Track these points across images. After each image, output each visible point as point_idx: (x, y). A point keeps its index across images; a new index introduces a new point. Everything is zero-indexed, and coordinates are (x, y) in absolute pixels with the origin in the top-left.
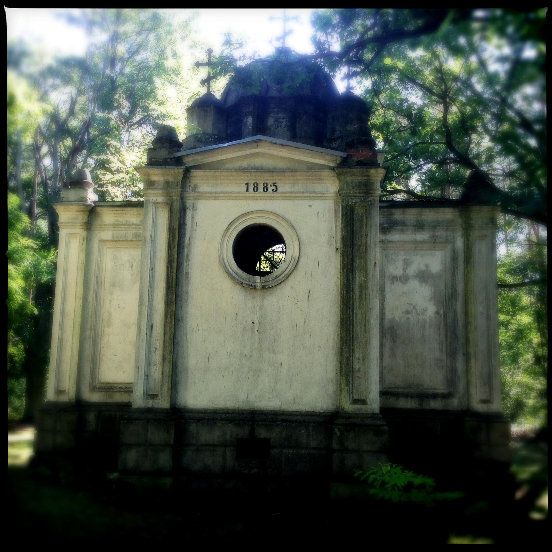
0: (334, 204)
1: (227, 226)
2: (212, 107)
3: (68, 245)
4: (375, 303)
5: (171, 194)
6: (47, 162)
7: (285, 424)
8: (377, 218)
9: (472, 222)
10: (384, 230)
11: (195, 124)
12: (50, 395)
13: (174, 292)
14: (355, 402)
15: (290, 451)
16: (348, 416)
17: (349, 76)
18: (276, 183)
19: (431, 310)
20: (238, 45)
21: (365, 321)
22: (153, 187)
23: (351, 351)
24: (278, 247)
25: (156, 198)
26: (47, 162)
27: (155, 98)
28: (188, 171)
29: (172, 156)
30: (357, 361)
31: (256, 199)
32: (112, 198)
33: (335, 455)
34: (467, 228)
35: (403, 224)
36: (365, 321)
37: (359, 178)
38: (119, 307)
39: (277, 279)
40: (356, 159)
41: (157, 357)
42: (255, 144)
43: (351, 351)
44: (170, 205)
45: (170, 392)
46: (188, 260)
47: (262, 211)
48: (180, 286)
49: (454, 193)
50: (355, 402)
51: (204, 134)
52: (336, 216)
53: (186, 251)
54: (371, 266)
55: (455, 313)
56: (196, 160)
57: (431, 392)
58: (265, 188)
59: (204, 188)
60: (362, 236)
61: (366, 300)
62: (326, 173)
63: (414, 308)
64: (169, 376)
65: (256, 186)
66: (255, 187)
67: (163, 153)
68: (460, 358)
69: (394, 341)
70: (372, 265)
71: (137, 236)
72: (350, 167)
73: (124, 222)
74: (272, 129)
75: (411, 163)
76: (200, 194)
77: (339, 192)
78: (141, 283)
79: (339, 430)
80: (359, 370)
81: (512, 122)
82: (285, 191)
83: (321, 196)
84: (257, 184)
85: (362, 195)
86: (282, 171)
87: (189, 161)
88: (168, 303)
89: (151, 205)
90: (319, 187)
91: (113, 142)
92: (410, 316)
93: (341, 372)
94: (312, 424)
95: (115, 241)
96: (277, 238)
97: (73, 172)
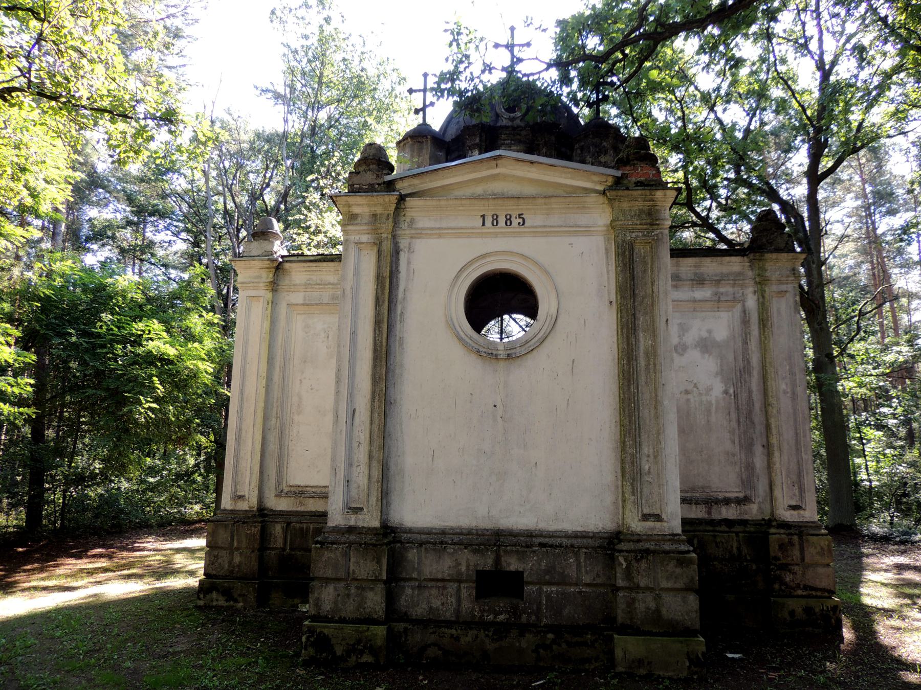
0: (605, 241)
1: (455, 274)
2: (429, 137)
5: (379, 231)
7: (544, 549)
9: (768, 274)
13: (384, 363)
14: (646, 517)
15: (553, 589)
16: (638, 538)
18: (522, 214)
19: (718, 388)
21: (656, 403)
22: (355, 222)
23: (638, 445)
25: (359, 236)
28: (402, 198)
29: (381, 181)
30: (646, 459)
31: (496, 235)
33: (621, 595)
34: (761, 282)
36: (656, 403)
38: (312, 389)
39: (527, 346)
40: (633, 179)
41: (361, 455)
42: (494, 163)
43: (638, 444)
44: (378, 244)
45: (379, 503)
46: (402, 321)
48: (392, 357)
50: (646, 517)
52: (607, 257)
53: (399, 308)
55: (750, 392)
56: (414, 185)
57: (721, 496)
58: (508, 222)
60: (646, 284)
61: (655, 373)
62: (593, 199)
63: (695, 386)
64: (378, 482)
65: (495, 218)
66: (494, 219)
67: (369, 177)
68: (758, 450)
70: (663, 324)
72: (627, 189)
73: (318, 282)
76: (419, 231)
77: (612, 225)
79: (626, 560)
80: (649, 472)
82: (535, 224)
83: (587, 231)
84: (497, 216)
85: (645, 227)
87: (404, 187)
88: (375, 381)
89: (353, 245)
90: (583, 219)
92: (689, 396)
93: (623, 476)
94: (584, 550)
95: (308, 304)
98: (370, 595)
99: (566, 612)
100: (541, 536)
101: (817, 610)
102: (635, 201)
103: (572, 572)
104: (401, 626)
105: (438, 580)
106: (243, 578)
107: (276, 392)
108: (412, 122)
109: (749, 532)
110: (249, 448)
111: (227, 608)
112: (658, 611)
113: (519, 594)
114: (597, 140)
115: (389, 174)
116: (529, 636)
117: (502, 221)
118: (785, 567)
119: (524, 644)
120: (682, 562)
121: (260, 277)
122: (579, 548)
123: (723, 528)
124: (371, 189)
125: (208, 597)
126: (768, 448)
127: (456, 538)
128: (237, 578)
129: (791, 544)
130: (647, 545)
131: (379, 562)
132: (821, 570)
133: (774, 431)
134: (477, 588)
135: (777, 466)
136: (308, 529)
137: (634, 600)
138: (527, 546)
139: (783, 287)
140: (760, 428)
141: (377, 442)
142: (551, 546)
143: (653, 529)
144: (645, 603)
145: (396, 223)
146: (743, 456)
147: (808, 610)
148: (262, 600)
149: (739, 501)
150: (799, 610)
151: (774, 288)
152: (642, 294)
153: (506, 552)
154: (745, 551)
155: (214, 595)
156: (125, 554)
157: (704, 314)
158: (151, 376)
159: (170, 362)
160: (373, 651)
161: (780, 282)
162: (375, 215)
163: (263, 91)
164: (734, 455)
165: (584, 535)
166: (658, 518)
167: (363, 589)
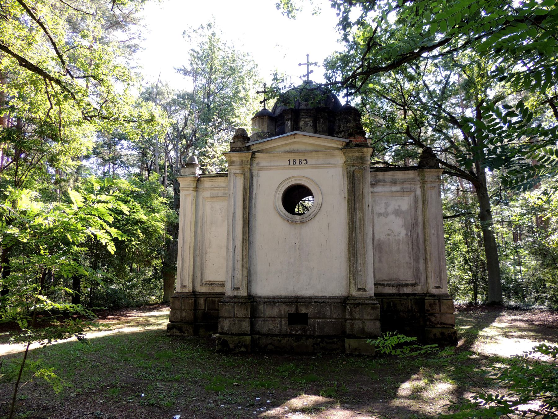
3: (185, 200)
4: (369, 230)
6: (172, 154)
8: (369, 178)
10: (373, 185)
11: (257, 127)
12: (178, 288)
14: (359, 290)
16: (355, 298)
17: (347, 95)
19: (403, 232)
20: (281, 81)
23: (356, 259)
24: (310, 197)
26: (172, 154)
27: (233, 114)
28: (254, 153)
29: (244, 146)
31: (295, 169)
32: (209, 172)
34: (423, 182)
35: (384, 181)
37: (357, 154)
40: (354, 143)
41: (239, 266)
42: (293, 137)
44: (244, 174)
46: (255, 207)
47: (299, 176)
49: (413, 163)
50: (359, 290)
51: (263, 132)
53: (254, 201)
54: (366, 207)
55: (418, 234)
57: (404, 283)
58: (300, 162)
59: (263, 163)
62: (337, 152)
63: (392, 232)
65: (295, 161)
67: (239, 144)
68: (422, 261)
69: (380, 252)
70: (367, 207)
71: (224, 194)
72: (351, 148)
74: (303, 127)
75: (385, 146)
78: (228, 222)
80: (361, 271)
81: (445, 118)
83: (334, 166)
86: (311, 152)
88: (244, 233)
89: (233, 175)
90: (333, 161)
91: (210, 141)
92: (390, 237)
96: (308, 192)
97: (187, 159)
98: (244, 323)
99: (326, 330)
100: (315, 298)
101: (446, 334)
102: (355, 153)
103: (328, 313)
104: (257, 337)
105: (272, 317)
106: (187, 322)
107: (199, 239)
108: (258, 108)
109: (416, 299)
110: (188, 264)
111: (181, 336)
112: (363, 328)
113: (306, 323)
114: (346, 116)
115: (248, 143)
116: (310, 340)
117: (297, 162)
118: (432, 314)
119: (308, 343)
120: (373, 308)
121: (190, 185)
122: (331, 303)
123: (405, 297)
124: (240, 150)
125: (172, 331)
126: (425, 260)
127: (279, 300)
128: (184, 323)
129: (435, 304)
130: (359, 301)
131: (247, 310)
132: (448, 316)
133: (428, 252)
134: (289, 321)
135: (429, 269)
136: (215, 300)
137: (353, 324)
138: (309, 303)
139: (433, 185)
140: (422, 251)
141: (245, 260)
142: (319, 302)
143: (362, 294)
144: (358, 325)
145: (251, 164)
146: (415, 264)
147: (442, 334)
148: (196, 332)
149: (412, 285)
150: (438, 334)
151: (429, 185)
152: (358, 194)
153: (300, 305)
154: (414, 307)
155: (174, 330)
156: (124, 318)
157: (396, 198)
158: (136, 230)
159: (144, 223)
160: (246, 346)
161: (432, 182)
162: (242, 161)
163: (178, 70)
164: (410, 264)
165: (334, 298)
166: (364, 290)
167: (241, 321)
